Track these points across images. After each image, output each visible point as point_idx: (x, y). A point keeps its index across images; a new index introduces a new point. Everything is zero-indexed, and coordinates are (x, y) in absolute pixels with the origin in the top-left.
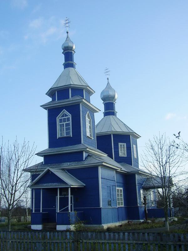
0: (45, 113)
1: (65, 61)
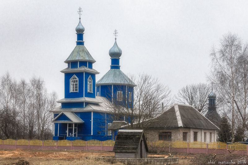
0: (63, 74)
1: (78, 40)
